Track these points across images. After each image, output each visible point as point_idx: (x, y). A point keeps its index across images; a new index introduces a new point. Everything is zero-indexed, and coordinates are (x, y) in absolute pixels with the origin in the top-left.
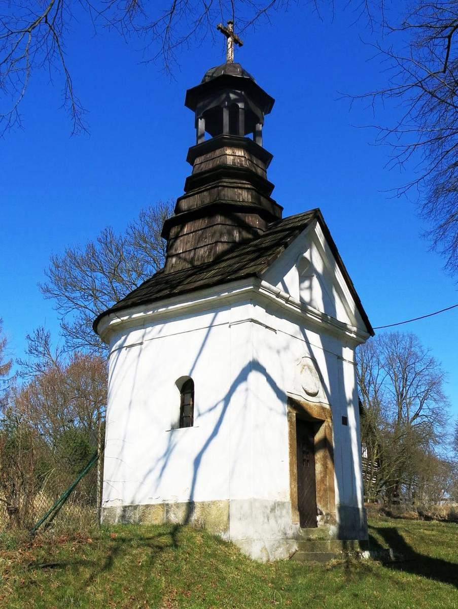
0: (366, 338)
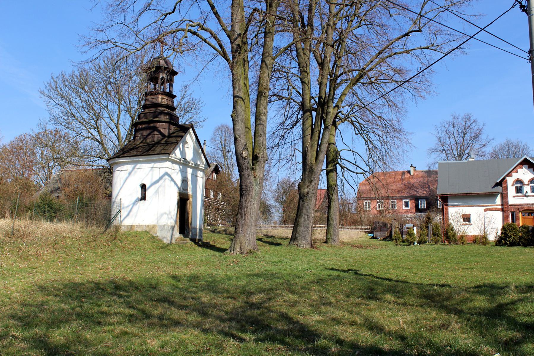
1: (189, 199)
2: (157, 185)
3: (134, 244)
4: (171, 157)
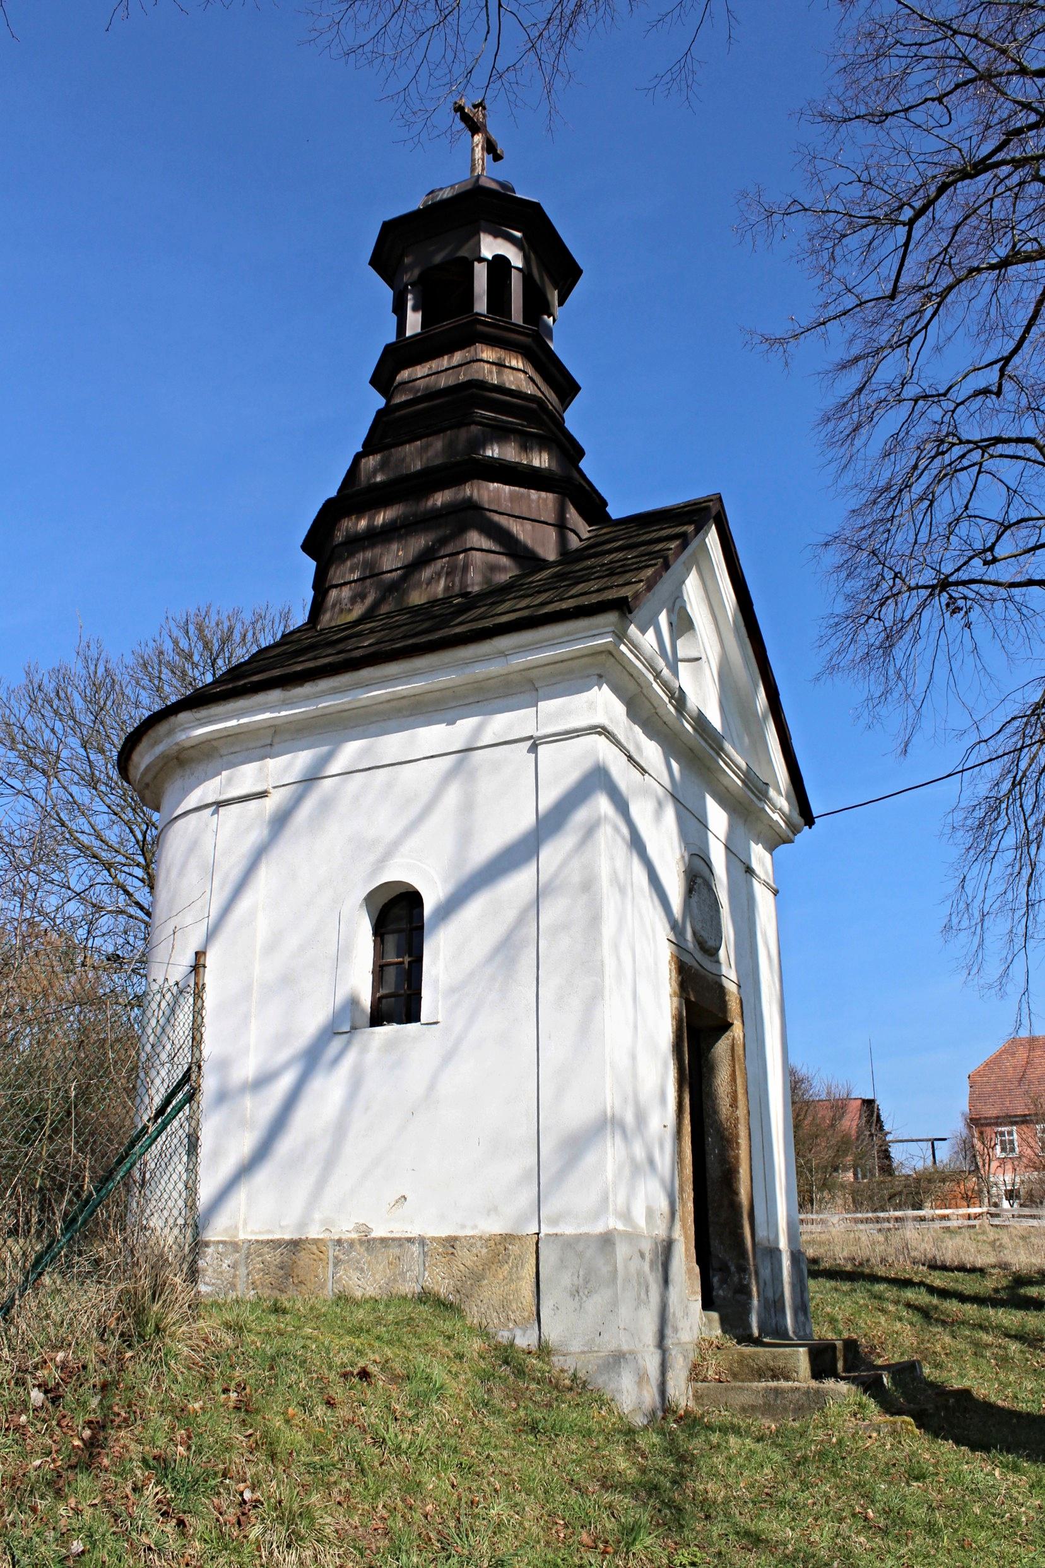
0: (796, 830)
1: (732, 1024)
2: (519, 883)
3: (346, 1502)
4: (635, 647)
